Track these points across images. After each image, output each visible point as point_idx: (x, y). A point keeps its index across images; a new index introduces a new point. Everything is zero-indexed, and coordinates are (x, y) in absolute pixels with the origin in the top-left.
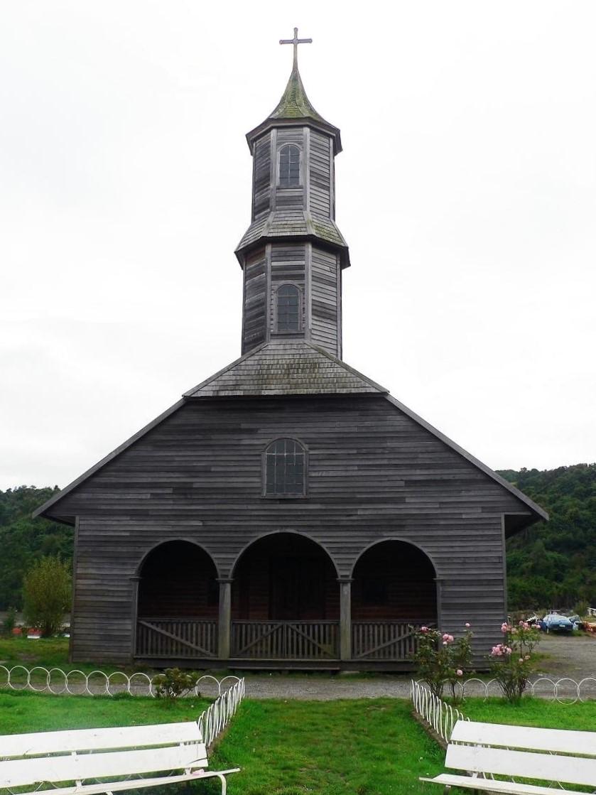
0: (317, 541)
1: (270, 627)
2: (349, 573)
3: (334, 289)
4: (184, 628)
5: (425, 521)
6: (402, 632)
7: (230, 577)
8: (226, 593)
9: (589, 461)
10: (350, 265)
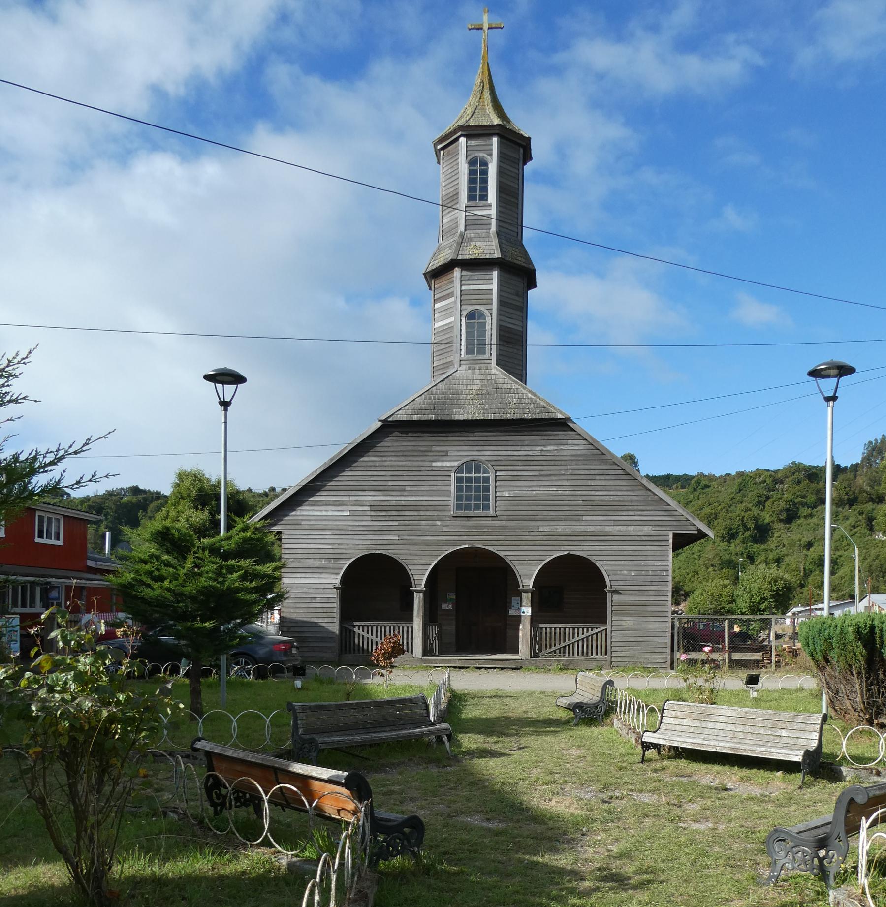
0: (501, 554)
1: (585, 630)
2: (531, 583)
3: (520, 314)
4: (383, 630)
5: (601, 537)
6: (576, 635)
7: (423, 586)
8: (418, 601)
9: (875, 435)
10: (535, 286)
